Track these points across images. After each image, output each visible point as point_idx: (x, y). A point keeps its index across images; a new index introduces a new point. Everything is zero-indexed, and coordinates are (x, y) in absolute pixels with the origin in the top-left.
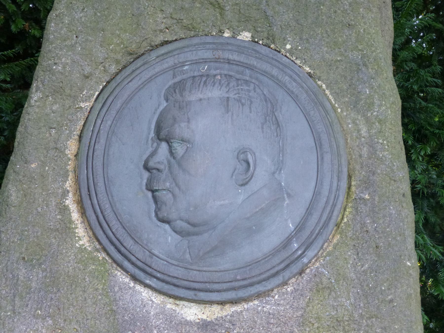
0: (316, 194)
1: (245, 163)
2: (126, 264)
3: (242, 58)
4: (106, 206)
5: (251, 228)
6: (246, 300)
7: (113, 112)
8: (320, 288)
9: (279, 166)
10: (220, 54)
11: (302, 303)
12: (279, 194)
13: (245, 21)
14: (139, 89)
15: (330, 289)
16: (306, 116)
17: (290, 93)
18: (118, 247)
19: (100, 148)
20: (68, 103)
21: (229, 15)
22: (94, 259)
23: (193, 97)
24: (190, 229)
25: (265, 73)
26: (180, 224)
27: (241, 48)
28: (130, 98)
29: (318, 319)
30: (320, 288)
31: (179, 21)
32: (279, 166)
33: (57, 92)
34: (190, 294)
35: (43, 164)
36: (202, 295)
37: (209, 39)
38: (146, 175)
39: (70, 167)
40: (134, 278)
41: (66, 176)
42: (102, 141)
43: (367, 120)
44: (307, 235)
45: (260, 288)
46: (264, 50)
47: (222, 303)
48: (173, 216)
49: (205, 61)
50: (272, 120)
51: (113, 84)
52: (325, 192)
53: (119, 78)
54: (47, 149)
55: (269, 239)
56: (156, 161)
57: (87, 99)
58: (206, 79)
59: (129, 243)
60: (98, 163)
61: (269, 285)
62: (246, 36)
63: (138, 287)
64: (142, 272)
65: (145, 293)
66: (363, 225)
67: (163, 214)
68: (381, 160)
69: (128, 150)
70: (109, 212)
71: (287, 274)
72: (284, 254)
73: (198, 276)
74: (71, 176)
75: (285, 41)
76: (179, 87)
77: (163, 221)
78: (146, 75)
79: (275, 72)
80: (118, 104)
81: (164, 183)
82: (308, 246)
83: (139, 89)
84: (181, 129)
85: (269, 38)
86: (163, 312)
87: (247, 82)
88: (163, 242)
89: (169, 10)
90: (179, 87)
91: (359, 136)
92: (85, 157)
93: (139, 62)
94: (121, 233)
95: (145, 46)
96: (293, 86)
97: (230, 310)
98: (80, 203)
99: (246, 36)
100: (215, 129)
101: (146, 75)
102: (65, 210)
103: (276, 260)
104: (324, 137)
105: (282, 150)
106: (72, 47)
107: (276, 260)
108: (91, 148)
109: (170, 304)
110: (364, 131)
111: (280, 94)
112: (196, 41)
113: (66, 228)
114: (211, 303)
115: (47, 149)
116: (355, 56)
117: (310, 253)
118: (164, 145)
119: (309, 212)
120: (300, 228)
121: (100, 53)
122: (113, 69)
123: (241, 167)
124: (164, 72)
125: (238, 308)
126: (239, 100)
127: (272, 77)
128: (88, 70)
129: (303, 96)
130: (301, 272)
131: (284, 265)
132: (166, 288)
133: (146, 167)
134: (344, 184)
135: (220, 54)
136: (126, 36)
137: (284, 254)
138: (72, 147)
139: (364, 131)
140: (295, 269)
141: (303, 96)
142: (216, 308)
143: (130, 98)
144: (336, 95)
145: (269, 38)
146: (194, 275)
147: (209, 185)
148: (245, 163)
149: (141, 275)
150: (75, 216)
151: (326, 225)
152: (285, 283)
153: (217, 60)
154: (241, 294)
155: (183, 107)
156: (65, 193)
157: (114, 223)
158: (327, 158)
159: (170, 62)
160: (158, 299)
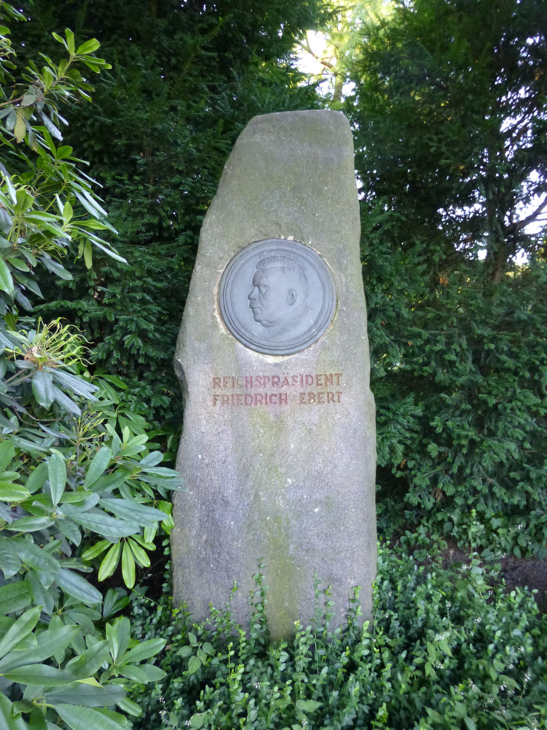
0: (323, 308)
1: (292, 295)
2: (242, 340)
3: (290, 249)
4: (233, 315)
5: (295, 323)
6: (293, 354)
7: (233, 274)
8: (324, 348)
9: (307, 296)
10: (280, 247)
11: (317, 355)
12: (307, 308)
13: (291, 231)
14: (244, 264)
15: (329, 349)
16: (319, 276)
17: (311, 264)
18: (238, 333)
19: (229, 290)
20: (213, 270)
21: (283, 228)
22: (228, 338)
23: (269, 266)
24: (269, 324)
25: (300, 255)
26: (264, 322)
27: (289, 244)
28: (240, 269)
29: (324, 361)
30: (324, 348)
31: (261, 232)
32: (307, 296)
33: (208, 265)
34: (269, 352)
35: (204, 298)
36: (275, 352)
37: (275, 240)
38: (249, 301)
39: (216, 298)
40: (246, 346)
41: (214, 303)
42: (230, 287)
43: (345, 275)
44: (319, 325)
45: (299, 349)
46: (299, 245)
47: (283, 355)
48: (261, 318)
49: (273, 250)
50: (304, 276)
51: (233, 262)
52: (327, 305)
53: (235, 259)
54: (205, 291)
55: (303, 327)
56: (147, 424)
57: (222, 268)
58: (274, 258)
59: (243, 331)
60: (228, 297)
61: (303, 347)
62: (291, 238)
63: (247, 350)
64: (249, 343)
65: (251, 352)
66: (343, 321)
67: (258, 318)
68: (352, 293)
69: (241, 291)
70: (234, 318)
71: (310, 342)
72: (309, 334)
73: (273, 344)
74: (216, 303)
75: (308, 240)
76: (262, 262)
77: (257, 321)
78: (248, 257)
79: (304, 255)
80: (236, 270)
81: (257, 305)
82: (319, 330)
83: (244, 264)
84: (264, 281)
85: (301, 239)
86: (258, 360)
87: (292, 260)
88: (258, 330)
89: (256, 227)
90: (262, 262)
91: (342, 282)
92: (222, 294)
93: (244, 252)
94: (239, 327)
95: (246, 244)
96: (312, 261)
97: (286, 358)
98: (221, 314)
99: (291, 238)
100: (278, 280)
101: (248, 257)
102: (214, 317)
103: (306, 337)
104: (326, 283)
105: (308, 289)
106: (213, 245)
107: (306, 337)
108: (225, 290)
109: (261, 356)
110: (344, 280)
111: (307, 265)
112: (269, 241)
113: (215, 326)
114: (278, 355)
115: (205, 291)
116: (341, 246)
117: (320, 333)
118: (257, 288)
119: (320, 315)
120: (316, 323)
121: (226, 248)
122: (232, 254)
123: (290, 297)
124: (255, 256)
125: (290, 357)
126: (289, 268)
127: (303, 257)
128: (221, 255)
129: (317, 265)
130: (316, 342)
131: (309, 339)
132: (259, 349)
133: (249, 298)
134: (335, 304)
135: (280, 247)
136: (237, 239)
137: (309, 334)
138: (215, 290)
139: (344, 280)
140: (314, 340)
141: (317, 265)
142: (280, 358)
143: (240, 269)
144: (332, 265)
145: (301, 239)
146: (271, 343)
147: (276, 306)
148: (292, 295)
149: (248, 344)
150: (219, 320)
151: (327, 321)
152: (310, 346)
153: (278, 250)
154: (291, 351)
155: (264, 271)
156: (214, 310)
157: (236, 322)
158: (327, 292)
159: (258, 251)
160: (256, 354)
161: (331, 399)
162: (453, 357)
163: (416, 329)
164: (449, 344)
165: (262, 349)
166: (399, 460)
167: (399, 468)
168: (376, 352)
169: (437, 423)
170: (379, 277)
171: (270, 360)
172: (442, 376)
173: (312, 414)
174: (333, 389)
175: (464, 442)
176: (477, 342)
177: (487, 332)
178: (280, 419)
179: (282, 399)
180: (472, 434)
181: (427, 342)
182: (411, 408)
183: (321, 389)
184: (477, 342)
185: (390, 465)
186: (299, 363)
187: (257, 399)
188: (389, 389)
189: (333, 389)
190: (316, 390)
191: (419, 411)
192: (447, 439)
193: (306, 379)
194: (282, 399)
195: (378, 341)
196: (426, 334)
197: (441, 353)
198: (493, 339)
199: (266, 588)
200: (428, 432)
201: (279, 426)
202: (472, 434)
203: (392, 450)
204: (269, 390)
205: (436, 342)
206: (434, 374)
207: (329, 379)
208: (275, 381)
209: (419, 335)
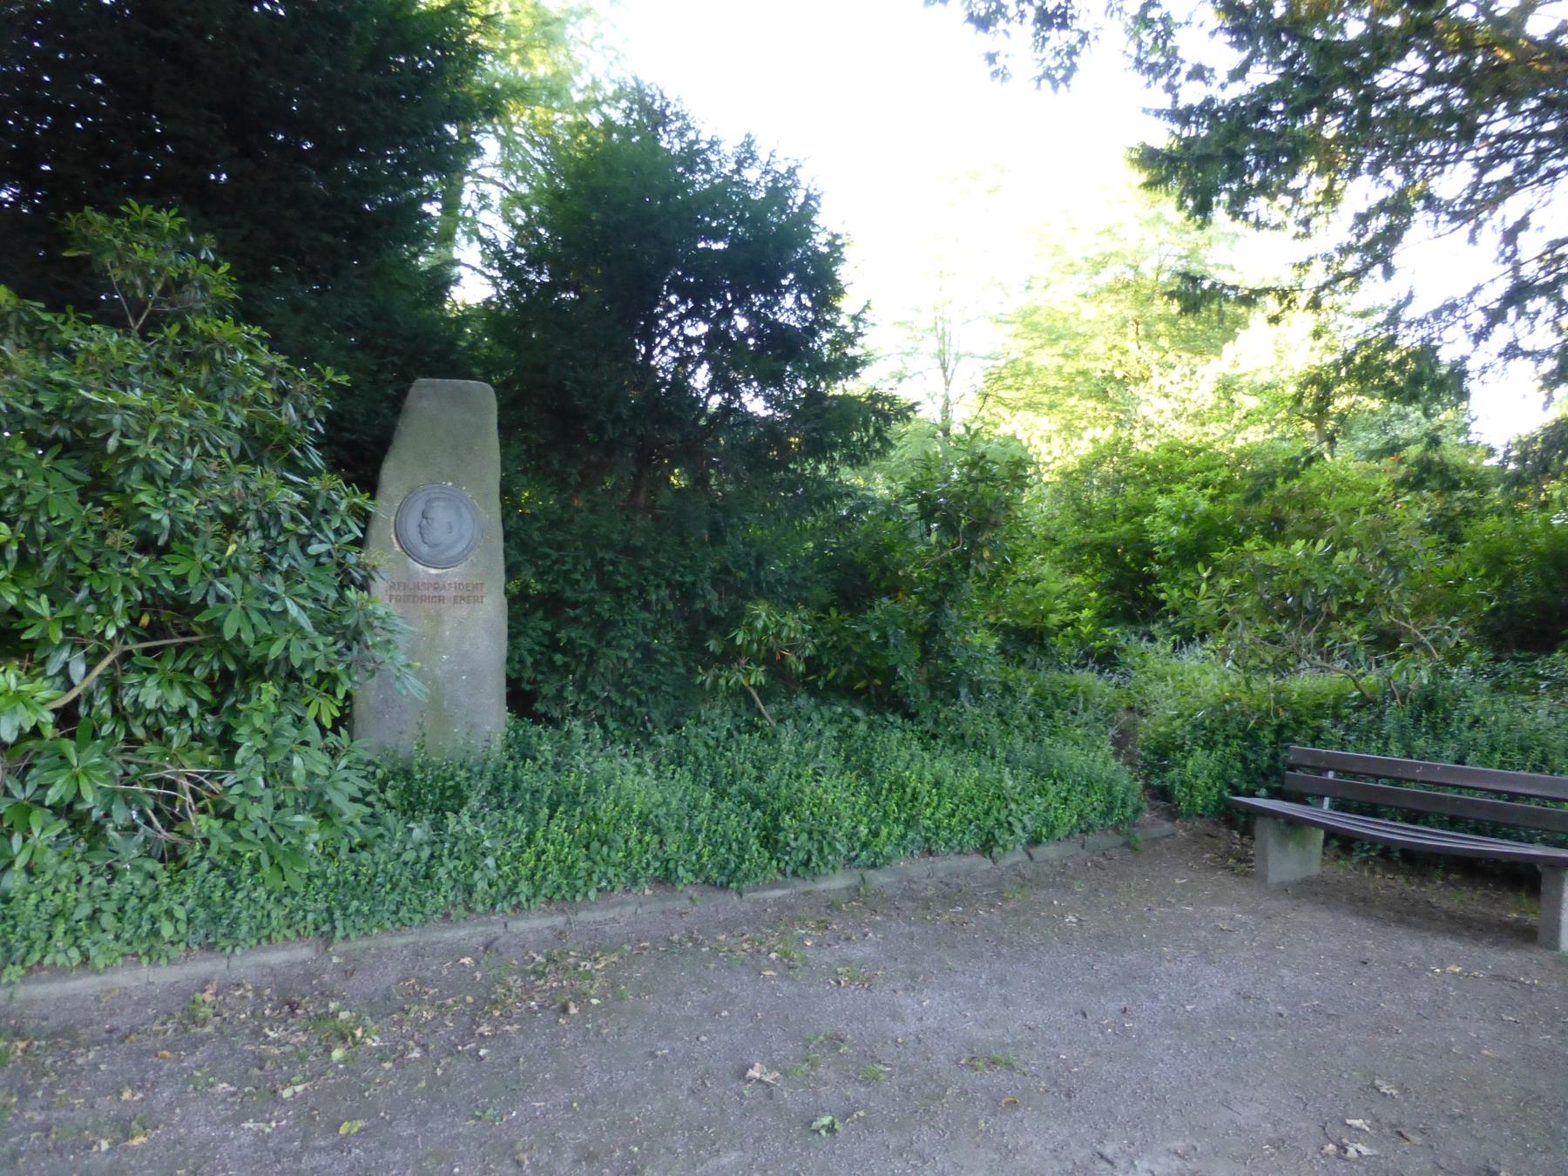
12: (461, 536)
24: (434, 546)
44: (469, 549)
64: (418, 558)
85: (457, 485)
88: (425, 549)
113: (391, 545)
131: (462, 557)
145: (457, 485)
147: (438, 532)
161: (476, 601)
162: (578, 576)
163: (547, 550)
164: (575, 565)
165: (427, 564)
166: (528, 674)
167: (529, 682)
168: (511, 571)
169: (562, 635)
170: (839, 908)
171: (433, 571)
172: (569, 593)
173: (463, 611)
174: (478, 594)
175: (584, 651)
176: (598, 565)
177: (609, 556)
178: (439, 615)
179: (441, 599)
180: (593, 644)
181: (556, 562)
182: (540, 624)
183: (469, 594)
184: (598, 565)
185: (520, 680)
186: (453, 575)
187: (422, 599)
188: (520, 606)
189: (478, 594)
190: (466, 594)
191: (547, 626)
192: (569, 649)
193: (459, 586)
194: (441, 599)
195: (512, 560)
196: (555, 555)
197: (568, 572)
198: (612, 563)
199: (426, 730)
200: (555, 646)
201: (438, 619)
202: (593, 644)
203: (522, 662)
204: (431, 592)
205: (564, 563)
206: (563, 591)
207: (475, 587)
208: (436, 587)
209: (547, 556)
